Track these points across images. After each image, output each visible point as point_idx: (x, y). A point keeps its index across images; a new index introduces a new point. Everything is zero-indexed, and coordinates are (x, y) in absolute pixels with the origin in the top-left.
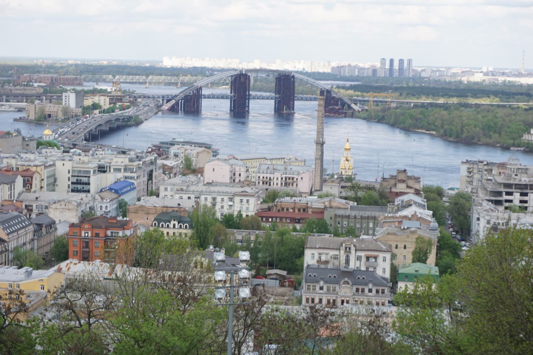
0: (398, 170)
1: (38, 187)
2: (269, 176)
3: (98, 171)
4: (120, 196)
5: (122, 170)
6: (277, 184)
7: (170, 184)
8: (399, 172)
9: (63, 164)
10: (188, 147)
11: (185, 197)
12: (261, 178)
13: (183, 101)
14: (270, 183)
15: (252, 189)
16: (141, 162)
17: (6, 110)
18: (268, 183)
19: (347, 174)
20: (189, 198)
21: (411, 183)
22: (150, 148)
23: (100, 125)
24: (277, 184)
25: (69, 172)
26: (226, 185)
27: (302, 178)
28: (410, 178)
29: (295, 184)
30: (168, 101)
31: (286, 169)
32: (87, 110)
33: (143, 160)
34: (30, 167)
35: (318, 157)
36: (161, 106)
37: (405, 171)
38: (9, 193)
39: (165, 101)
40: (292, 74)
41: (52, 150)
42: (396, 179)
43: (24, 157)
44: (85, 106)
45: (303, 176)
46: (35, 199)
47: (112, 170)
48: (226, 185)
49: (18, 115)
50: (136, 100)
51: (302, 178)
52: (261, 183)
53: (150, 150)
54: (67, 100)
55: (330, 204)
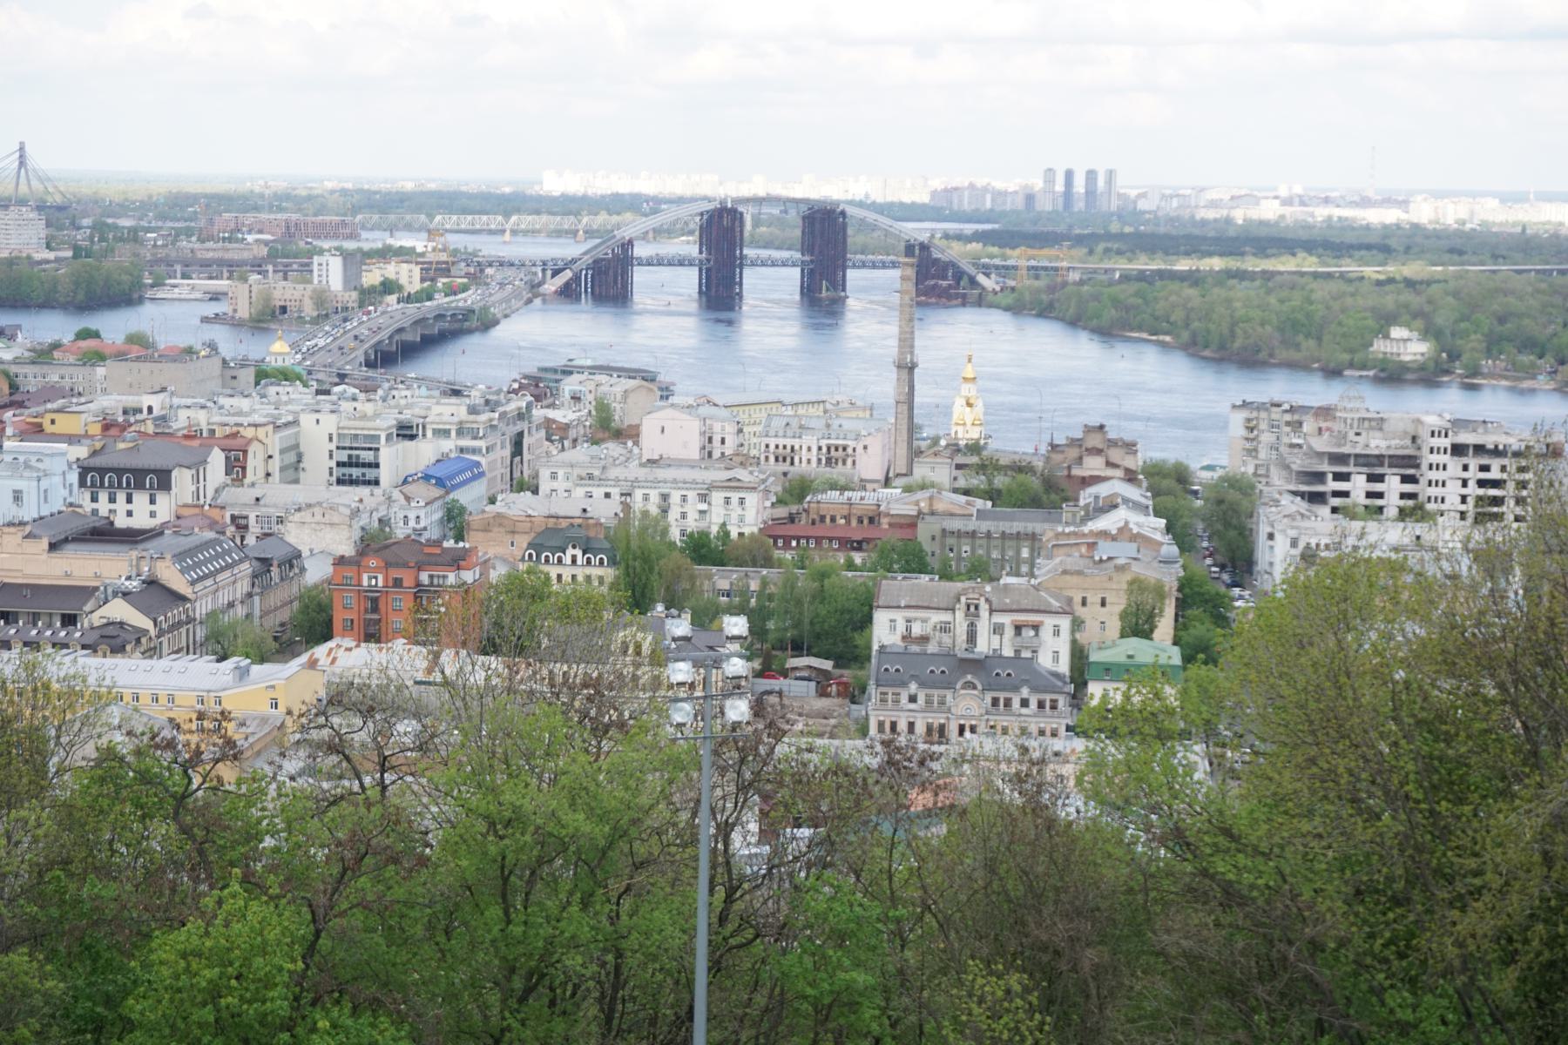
0: (1086, 426)
1: (262, 474)
2: (789, 442)
3: (398, 435)
4: (447, 493)
5: (453, 433)
6: (809, 461)
7: (564, 465)
8: (1089, 430)
9: (318, 421)
10: (603, 378)
11: (598, 492)
12: (772, 447)
13: (590, 272)
14: (792, 459)
15: (751, 473)
16: (496, 415)
17: (182, 296)
18: (789, 460)
19: (968, 436)
20: (607, 495)
21: (1116, 455)
22: (515, 381)
23: (400, 330)
24: (809, 461)
25: (331, 439)
26: (692, 465)
27: (865, 447)
28: (1113, 443)
29: (849, 461)
30: (556, 273)
31: (828, 426)
32: (370, 296)
33: (501, 409)
34: (241, 429)
35: (902, 398)
36: (540, 284)
37: (1102, 427)
38: (194, 488)
39: (549, 273)
40: (841, 208)
41: (290, 389)
42: (1080, 446)
43: (227, 407)
44: (365, 286)
45: (867, 441)
46: (253, 501)
47: (429, 433)
48: (692, 465)
49: (212, 309)
50: (482, 271)
51: (865, 447)
52: (772, 459)
53: (516, 386)
54: (324, 273)
55: (931, 505)
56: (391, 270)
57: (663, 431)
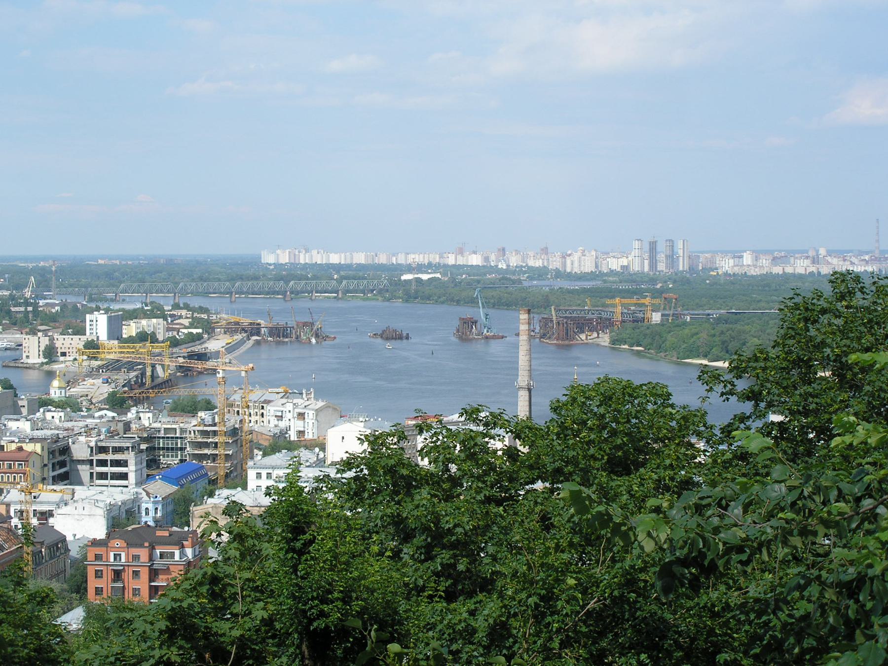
41: (62, 414)
56: (145, 324)
57: (343, 438)
